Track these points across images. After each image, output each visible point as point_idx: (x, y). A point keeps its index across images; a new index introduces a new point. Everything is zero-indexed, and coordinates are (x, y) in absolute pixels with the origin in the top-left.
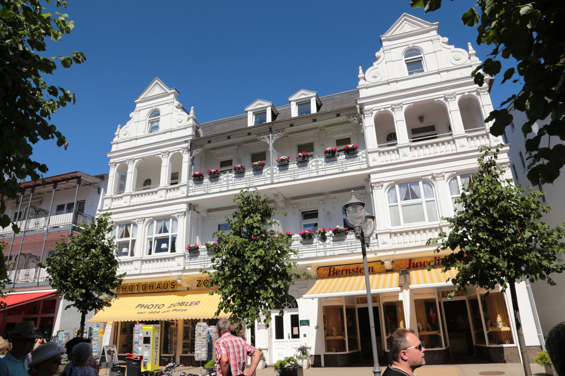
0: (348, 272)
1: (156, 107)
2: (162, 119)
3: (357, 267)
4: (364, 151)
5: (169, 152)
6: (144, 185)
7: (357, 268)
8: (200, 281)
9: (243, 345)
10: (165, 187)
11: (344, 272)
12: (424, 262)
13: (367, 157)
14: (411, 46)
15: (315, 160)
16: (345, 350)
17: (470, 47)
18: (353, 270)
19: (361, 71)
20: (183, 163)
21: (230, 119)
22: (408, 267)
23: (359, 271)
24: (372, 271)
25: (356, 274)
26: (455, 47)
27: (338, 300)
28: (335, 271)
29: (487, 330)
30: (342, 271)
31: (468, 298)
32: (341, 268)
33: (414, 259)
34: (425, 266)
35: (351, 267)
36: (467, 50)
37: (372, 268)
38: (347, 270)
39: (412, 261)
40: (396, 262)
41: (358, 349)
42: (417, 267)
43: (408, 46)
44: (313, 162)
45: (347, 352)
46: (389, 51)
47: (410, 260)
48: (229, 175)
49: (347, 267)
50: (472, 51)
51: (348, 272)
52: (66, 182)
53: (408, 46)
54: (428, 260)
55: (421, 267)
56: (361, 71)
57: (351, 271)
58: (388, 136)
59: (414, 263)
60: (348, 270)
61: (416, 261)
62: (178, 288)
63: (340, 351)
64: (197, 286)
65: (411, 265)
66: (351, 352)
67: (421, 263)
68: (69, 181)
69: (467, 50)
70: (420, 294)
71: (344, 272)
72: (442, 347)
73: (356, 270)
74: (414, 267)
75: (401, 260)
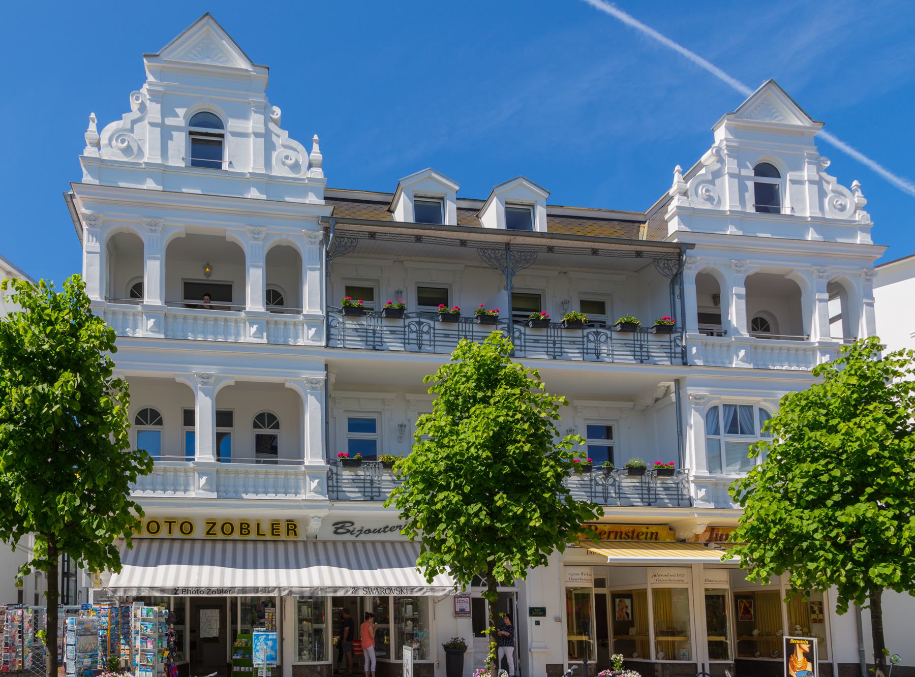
3: (631, 529)
7: (633, 532)
8: (214, 524)
9: (128, 643)
11: (612, 536)
15: (594, 330)
17: (316, 147)
18: (626, 534)
19: (92, 127)
21: (657, 208)
24: (656, 539)
26: (290, 136)
28: (598, 532)
30: (610, 533)
31: (611, 592)
32: (607, 528)
35: (624, 529)
36: (309, 150)
37: (657, 533)
38: (617, 533)
44: (589, 333)
48: (600, 330)
49: (616, 528)
50: (316, 154)
55: (716, 540)
56: (92, 127)
57: (624, 536)
58: (134, 287)
60: (619, 534)
62: (682, 535)
64: (208, 533)
69: (309, 150)
70: (713, 581)
71: (612, 536)
73: (630, 534)
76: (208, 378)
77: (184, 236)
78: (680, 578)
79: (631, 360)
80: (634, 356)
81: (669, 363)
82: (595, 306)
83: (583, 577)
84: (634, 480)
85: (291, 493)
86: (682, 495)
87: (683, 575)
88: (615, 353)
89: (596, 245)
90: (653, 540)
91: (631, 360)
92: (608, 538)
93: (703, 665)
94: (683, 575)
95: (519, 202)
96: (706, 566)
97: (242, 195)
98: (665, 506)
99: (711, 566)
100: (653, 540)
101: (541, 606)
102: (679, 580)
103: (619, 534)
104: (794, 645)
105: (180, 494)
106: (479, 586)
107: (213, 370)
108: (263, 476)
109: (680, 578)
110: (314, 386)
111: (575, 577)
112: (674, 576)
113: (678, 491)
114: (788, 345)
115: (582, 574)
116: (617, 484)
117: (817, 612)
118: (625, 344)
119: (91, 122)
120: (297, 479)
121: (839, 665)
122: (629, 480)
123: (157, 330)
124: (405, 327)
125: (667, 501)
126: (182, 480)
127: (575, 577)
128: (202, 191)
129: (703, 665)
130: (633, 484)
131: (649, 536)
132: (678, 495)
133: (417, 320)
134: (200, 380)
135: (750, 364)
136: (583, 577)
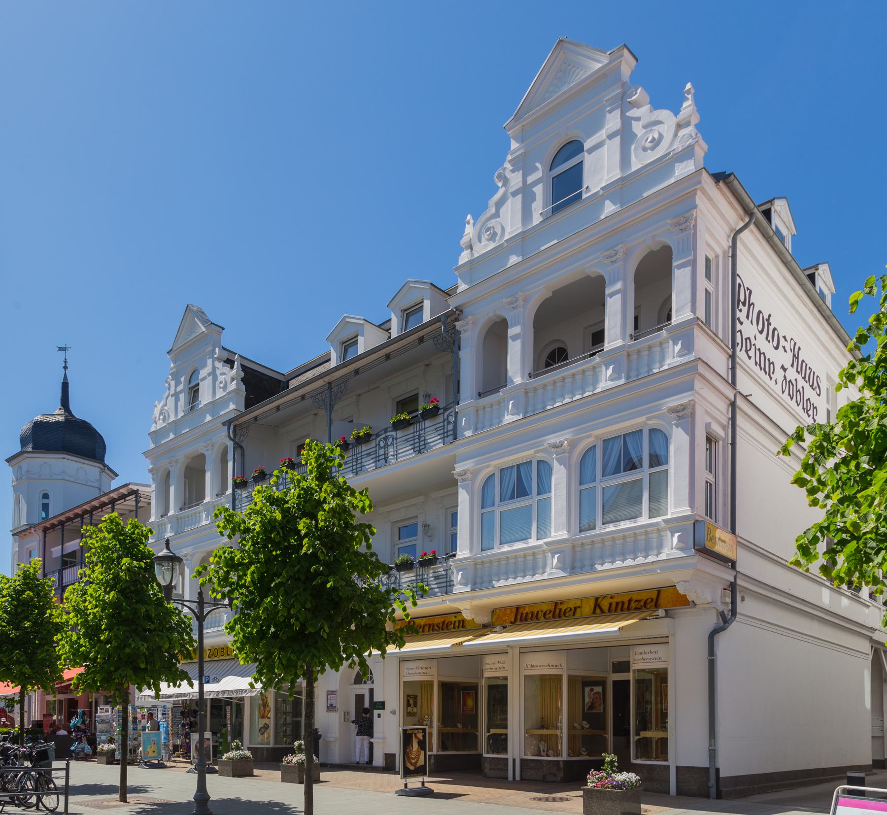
2: (588, 160)
3: (443, 620)
6: (548, 365)
7: (444, 622)
11: (427, 628)
12: (538, 612)
20: (510, 341)
22: (513, 620)
23: (445, 626)
24: (463, 627)
25: (441, 631)
27: (424, 673)
29: (637, 734)
32: (422, 622)
34: (537, 619)
38: (430, 625)
39: (521, 611)
41: (637, 757)
42: (526, 620)
45: (564, 757)
47: (518, 608)
52: (122, 501)
59: (522, 614)
60: (432, 626)
61: (527, 610)
63: (493, 753)
65: (519, 617)
66: (441, 753)
67: (532, 613)
68: (127, 499)
70: (534, 666)
71: (427, 628)
73: (441, 625)
74: (521, 620)
76: (683, 410)
77: (551, 294)
78: (500, 666)
79: (412, 454)
80: (414, 448)
81: (442, 445)
82: (407, 404)
83: (417, 671)
84: (411, 575)
85: (538, 574)
86: (450, 581)
87: (504, 662)
88: (399, 452)
89: (420, 334)
90: (461, 629)
91: (412, 454)
92: (574, 614)
93: (514, 760)
94: (504, 662)
95: (93, 468)
96: (523, 650)
97: (641, 195)
98: (434, 595)
99: (529, 650)
100: (461, 629)
101: (382, 700)
102: (499, 668)
103: (432, 626)
104: (411, 735)
105: (538, 577)
106: (361, 683)
107: (563, 437)
108: (644, 537)
109: (500, 666)
110: (680, 414)
111: (411, 671)
112: (495, 663)
113: (447, 578)
114: (572, 371)
115: (417, 668)
116: (398, 581)
117: (412, 706)
118: (406, 440)
119: (217, 369)
120: (545, 557)
121: (678, 768)
122: (407, 575)
123: (686, 352)
124: (444, 422)
125: (437, 590)
126: (654, 543)
127: (411, 671)
128: (558, 239)
129: (514, 760)
130: (410, 579)
131: (457, 624)
132: (446, 582)
133: (384, 436)
134: (673, 415)
135: (519, 415)
136: (417, 671)
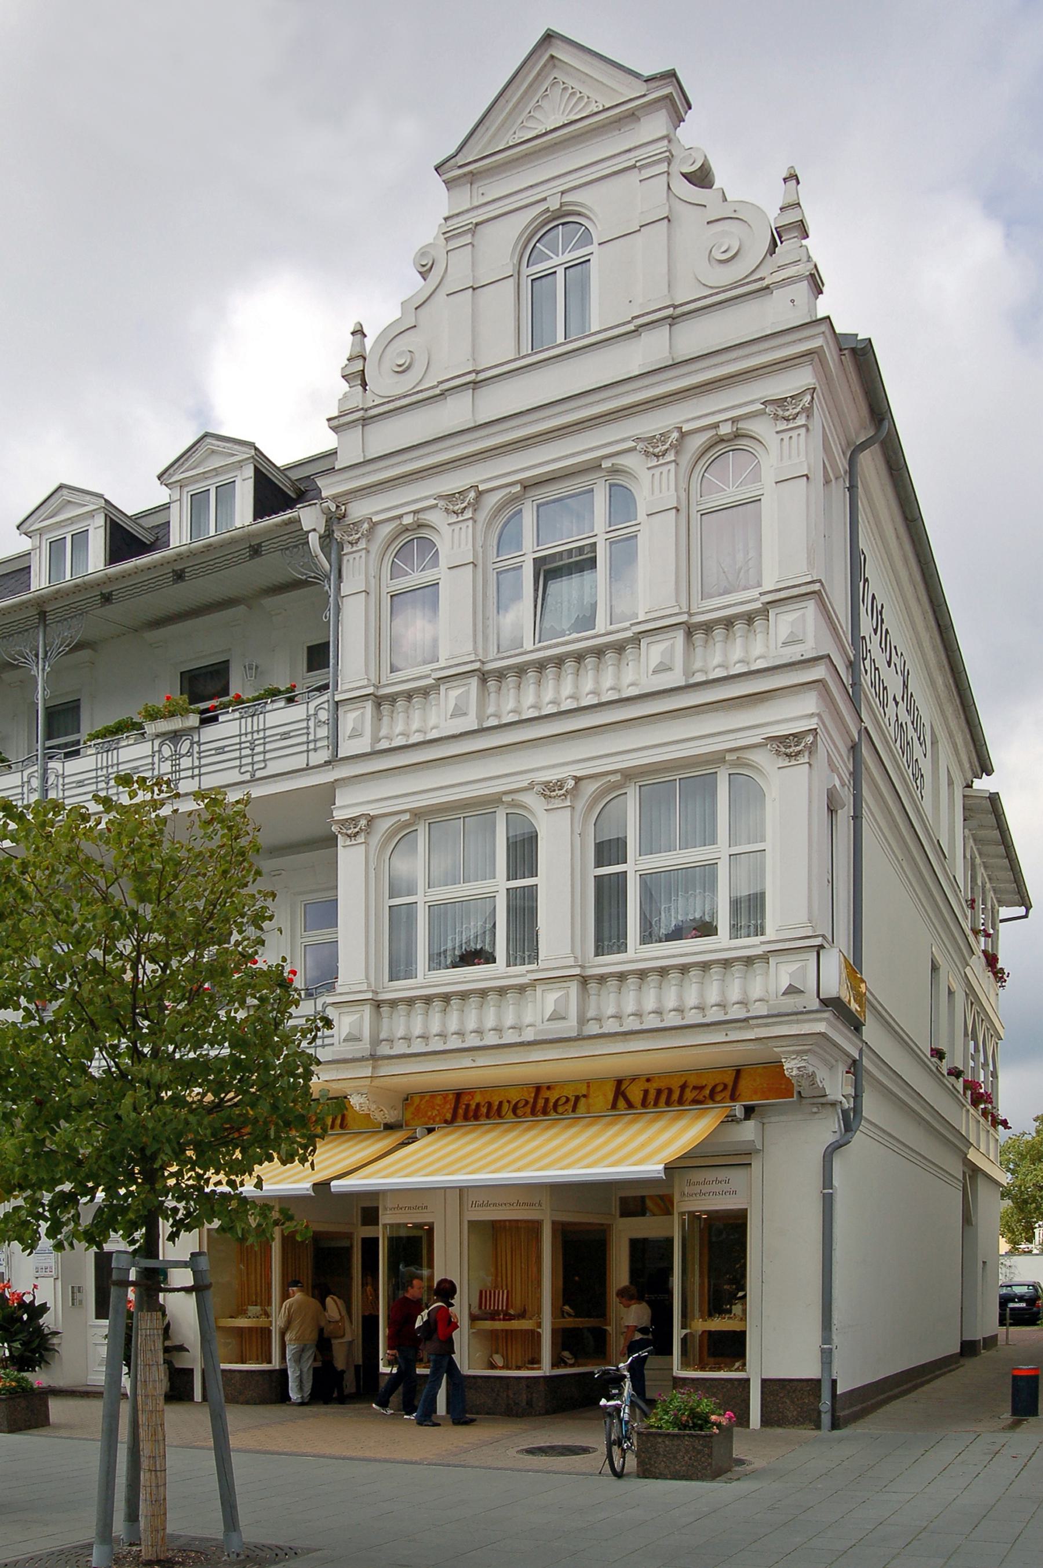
0: (676, 1096)
1: (567, 198)
4: (325, 698)
5: (374, 525)
10: (477, 665)
12: (501, 1103)
13: (335, 724)
14: (554, 204)
16: (535, 1361)
33: (470, 1092)
34: (500, 1116)
39: (465, 1100)
40: (417, 1100)
42: (476, 1118)
43: (542, 207)
45: (546, 1369)
46: (467, 239)
47: (459, 1095)
51: (676, 1096)
53: (542, 207)
54: (515, 1096)
55: (488, 1116)
59: (468, 1106)
61: (478, 1098)
65: (461, 1111)
67: (490, 1105)
72: (270, 1362)
75: (433, 1094)
